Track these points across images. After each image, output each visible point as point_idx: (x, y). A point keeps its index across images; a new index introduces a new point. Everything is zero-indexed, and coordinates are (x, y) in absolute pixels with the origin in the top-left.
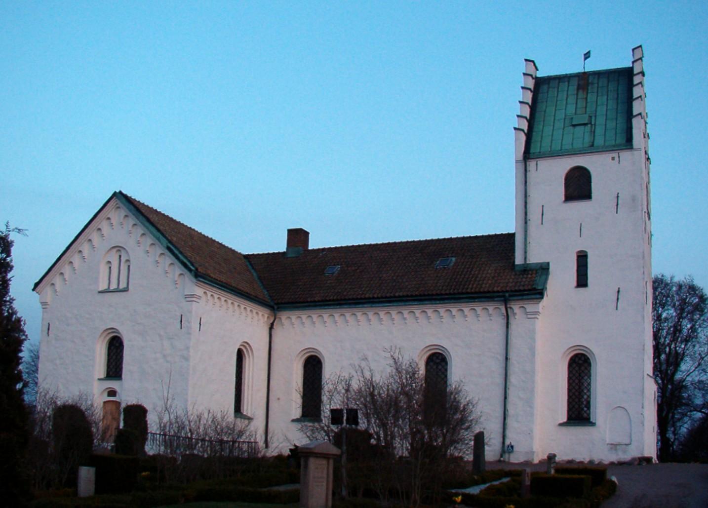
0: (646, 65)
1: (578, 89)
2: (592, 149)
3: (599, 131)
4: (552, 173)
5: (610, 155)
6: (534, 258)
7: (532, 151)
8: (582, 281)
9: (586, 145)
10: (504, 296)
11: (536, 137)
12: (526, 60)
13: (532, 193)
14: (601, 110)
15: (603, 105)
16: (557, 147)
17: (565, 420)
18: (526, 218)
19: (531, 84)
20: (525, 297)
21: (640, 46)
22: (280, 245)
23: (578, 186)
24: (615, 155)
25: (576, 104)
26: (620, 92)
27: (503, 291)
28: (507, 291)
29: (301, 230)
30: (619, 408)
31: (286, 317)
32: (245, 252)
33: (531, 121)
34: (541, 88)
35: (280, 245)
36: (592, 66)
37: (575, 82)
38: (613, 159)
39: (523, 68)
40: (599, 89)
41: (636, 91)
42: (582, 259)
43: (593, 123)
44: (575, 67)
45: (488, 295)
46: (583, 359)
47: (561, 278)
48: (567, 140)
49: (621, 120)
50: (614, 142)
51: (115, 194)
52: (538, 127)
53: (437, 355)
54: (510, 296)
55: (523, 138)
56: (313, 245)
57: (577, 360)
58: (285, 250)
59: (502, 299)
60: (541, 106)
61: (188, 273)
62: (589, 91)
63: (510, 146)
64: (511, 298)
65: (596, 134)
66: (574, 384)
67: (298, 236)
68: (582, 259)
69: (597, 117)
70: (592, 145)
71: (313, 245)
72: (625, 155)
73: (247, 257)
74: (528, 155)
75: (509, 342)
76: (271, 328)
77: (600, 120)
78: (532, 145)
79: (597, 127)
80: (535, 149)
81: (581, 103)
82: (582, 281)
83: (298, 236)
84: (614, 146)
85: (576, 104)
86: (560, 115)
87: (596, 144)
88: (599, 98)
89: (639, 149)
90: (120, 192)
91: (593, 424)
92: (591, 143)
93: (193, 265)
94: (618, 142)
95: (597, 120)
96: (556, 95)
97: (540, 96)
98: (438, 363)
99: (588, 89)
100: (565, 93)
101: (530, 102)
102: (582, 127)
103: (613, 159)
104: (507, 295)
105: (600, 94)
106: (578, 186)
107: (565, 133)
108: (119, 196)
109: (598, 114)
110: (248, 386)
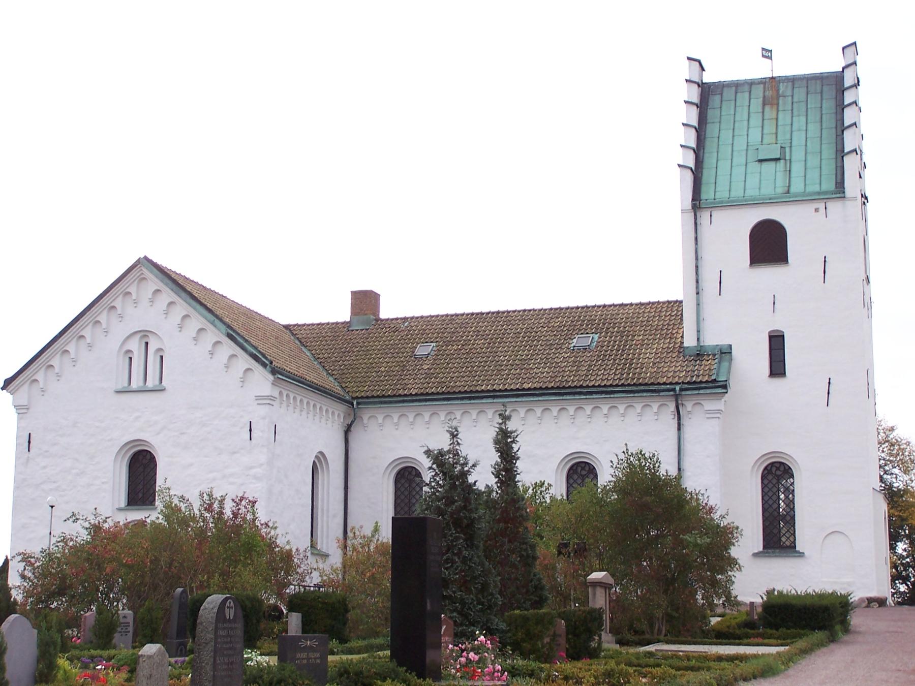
0: (862, 70)
1: (764, 104)
2: (787, 198)
3: (797, 169)
4: (732, 231)
5: (812, 207)
6: (712, 339)
7: (704, 196)
8: (777, 368)
9: (780, 190)
10: (674, 390)
11: (708, 175)
12: (689, 59)
13: (705, 254)
14: (798, 139)
15: (802, 131)
16: (737, 193)
17: (761, 549)
18: (697, 287)
19: (694, 95)
20: (702, 392)
21: (855, 43)
22: (341, 313)
23: (768, 245)
24: (821, 206)
25: (763, 112)
26: (825, 155)
27: (671, 383)
28: (677, 383)
29: (371, 292)
30: (832, 536)
31: (368, 415)
32: (284, 319)
33: (699, 151)
34: (708, 97)
35: (341, 313)
36: (783, 67)
37: (758, 91)
38: (817, 210)
39: (686, 71)
40: (795, 105)
41: (848, 98)
42: (777, 342)
43: (788, 158)
44: (761, 70)
45: (651, 388)
46: (782, 468)
47: (751, 359)
48: (753, 181)
49: (829, 152)
50: (818, 186)
51: (138, 262)
52: (710, 161)
53: (583, 465)
54: (681, 390)
55: (689, 176)
56: (385, 313)
57: (774, 469)
58: (348, 320)
59: (672, 393)
60: (712, 130)
61: (261, 368)
62: (781, 108)
63: (675, 190)
64: (683, 393)
65: (793, 174)
66: (770, 502)
67: (364, 302)
68: (777, 342)
69: (793, 148)
70: (788, 192)
71: (385, 313)
72: (835, 207)
73: (286, 327)
74: (697, 203)
75: (682, 447)
76: (347, 431)
77: (798, 155)
78: (704, 188)
79: (793, 164)
80: (707, 194)
81: (769, 128)
82: (777, 368)
83: (364, 302)
84: (819, 193)
85: (763, 112)
86: (740, 144)
87: (792, 190)
88: (794, 118)
89: (855, 199)
90: (146, 258)
91: (801, 555)
92: (786, 189)
93: (266, 358)
94: (825, 187)
95: (793, 153)
96: (733, 112)
97: (710, 113)
98: (583, 476)
99: (778, 104)
100: (746, 109)
101: (696, 124)
102: (773, 164)
103: (817, 210)
104: (678, 388)
105: (795, 113)
106: (768, 245)
107: (749, 171)
108: (146, 262)
109: (793, 144)
110: (323, 510)
